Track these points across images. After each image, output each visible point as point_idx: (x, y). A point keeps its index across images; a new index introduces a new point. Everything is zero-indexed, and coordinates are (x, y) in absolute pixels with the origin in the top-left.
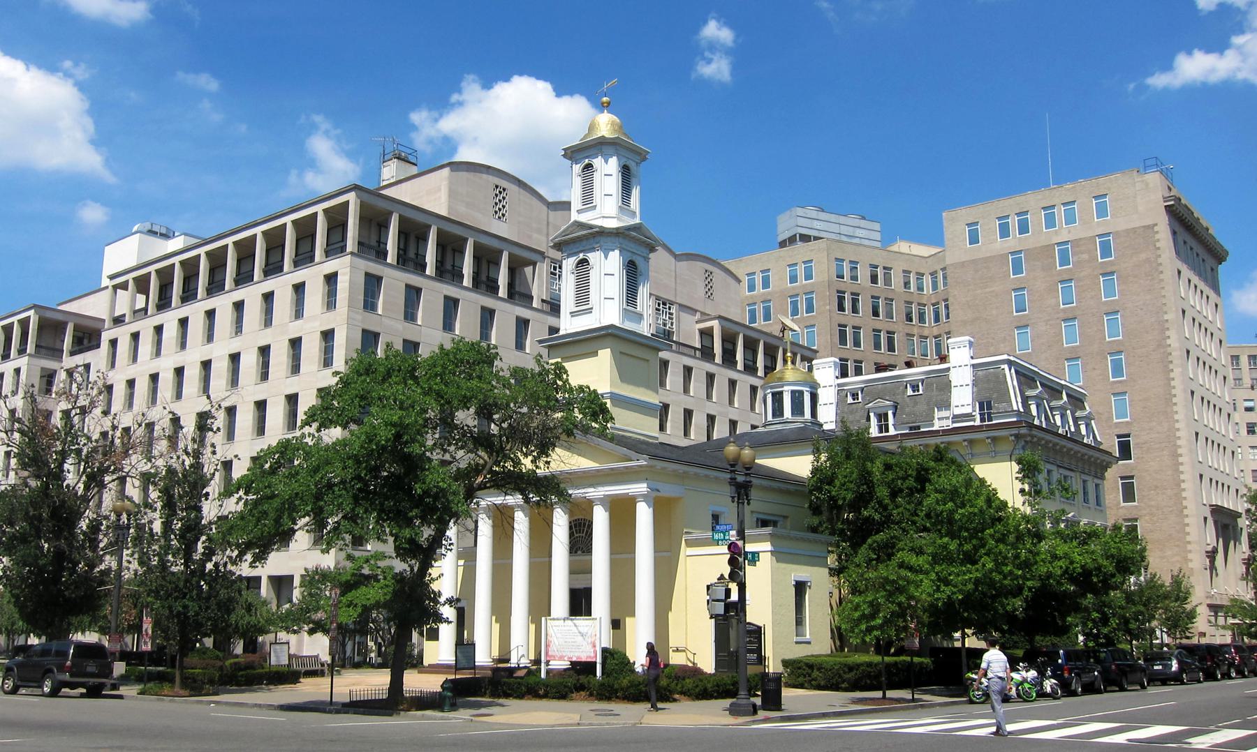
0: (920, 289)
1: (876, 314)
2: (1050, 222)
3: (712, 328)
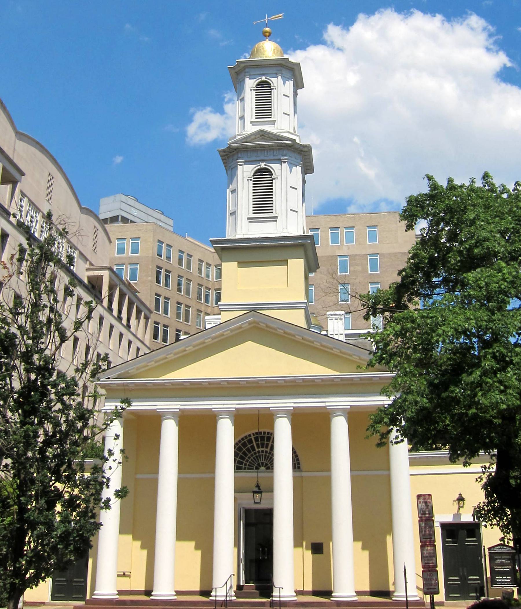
0: (208, 276)
1: (179, 290)
2: (335, 239)
3: (101, 277)
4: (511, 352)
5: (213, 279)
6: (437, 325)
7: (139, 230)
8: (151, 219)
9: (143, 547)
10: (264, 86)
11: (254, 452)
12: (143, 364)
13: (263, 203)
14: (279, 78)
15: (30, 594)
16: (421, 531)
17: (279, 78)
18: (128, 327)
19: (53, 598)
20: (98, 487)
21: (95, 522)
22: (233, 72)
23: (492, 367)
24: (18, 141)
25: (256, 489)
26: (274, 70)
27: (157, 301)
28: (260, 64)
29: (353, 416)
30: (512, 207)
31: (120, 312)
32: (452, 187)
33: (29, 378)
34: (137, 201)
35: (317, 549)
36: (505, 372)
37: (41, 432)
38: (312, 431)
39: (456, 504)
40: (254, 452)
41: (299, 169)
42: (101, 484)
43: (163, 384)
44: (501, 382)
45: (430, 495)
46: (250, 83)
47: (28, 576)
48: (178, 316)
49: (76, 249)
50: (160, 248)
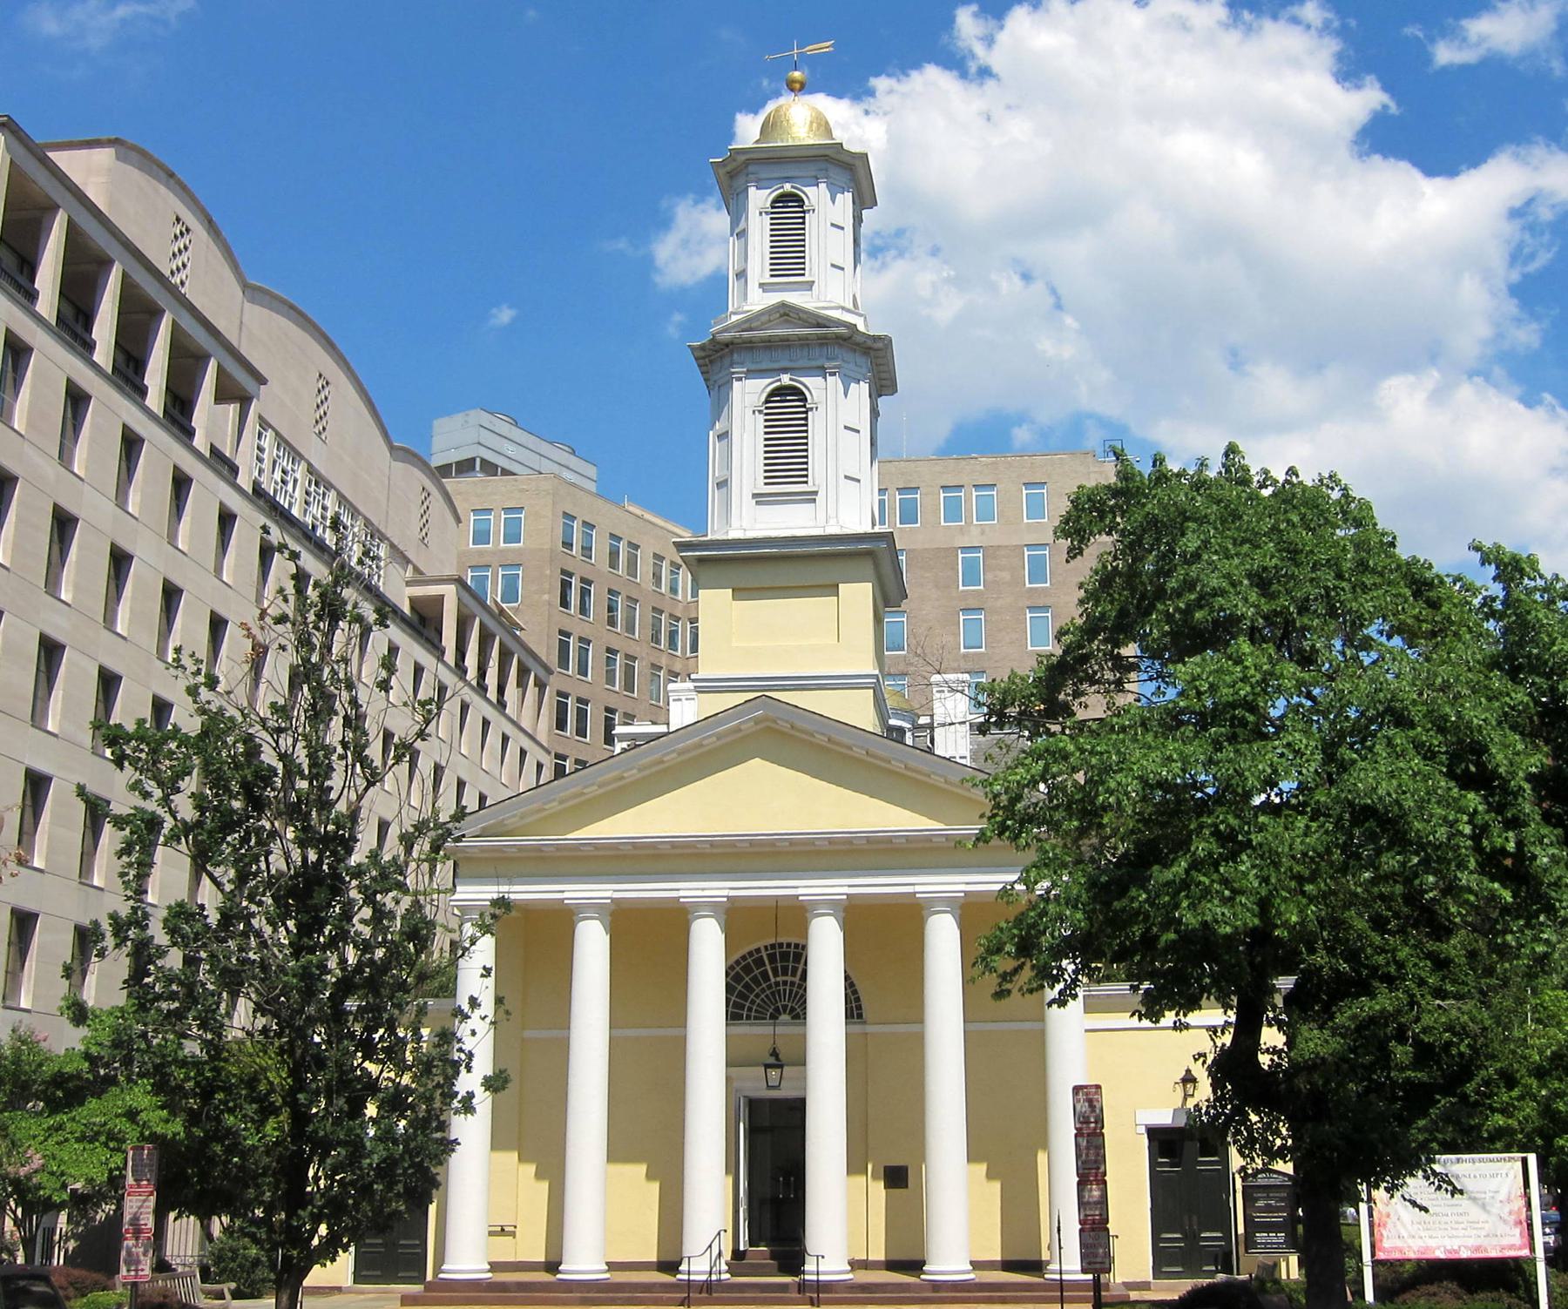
0: (674, 590)
1: (612, 622)
2: (953, 511)
4: (1249, 824)
5: (685, 596)
6: (1107, 770)
7: (522, 491)
8: (547, 466)
9: (539, 1176)
10: (789, 203)
11: (767, 983)
12: (535, 806)
13: (787, 460)
14: (823, 186)
15: (317, 1276)
16: (1078, 1156)
17: (823, 186)
18: (501, 704)
19: (358, 1278)
20: (450, 1071)
21: (443, 1139)
22: (722, 171)
23: (1210, 854)
24: (247, 305)
25: (772, 1060)
26: (811, 170)
27: (564, 648)
28: (778, 155)
29: (968, 911)
30: (1277, 521)
31: (482, 673)
32: (1161, 477)
33: (305, 859)
34: (516, 424)
35: (896, 1177)
36: (1235, 862)
37: (332, 963)
38: (884, 939)
39: (1179, 1088)
40: (767, 983)
41: (864, 387)
42: (456, 1065)
43: (576, 848)
44: (1225, 882)
45: (1098, 1087)
46: (759, 198)
47: (315, 1242)
48: (613, 563)
49: (383, 538)
50: (568, 530)
